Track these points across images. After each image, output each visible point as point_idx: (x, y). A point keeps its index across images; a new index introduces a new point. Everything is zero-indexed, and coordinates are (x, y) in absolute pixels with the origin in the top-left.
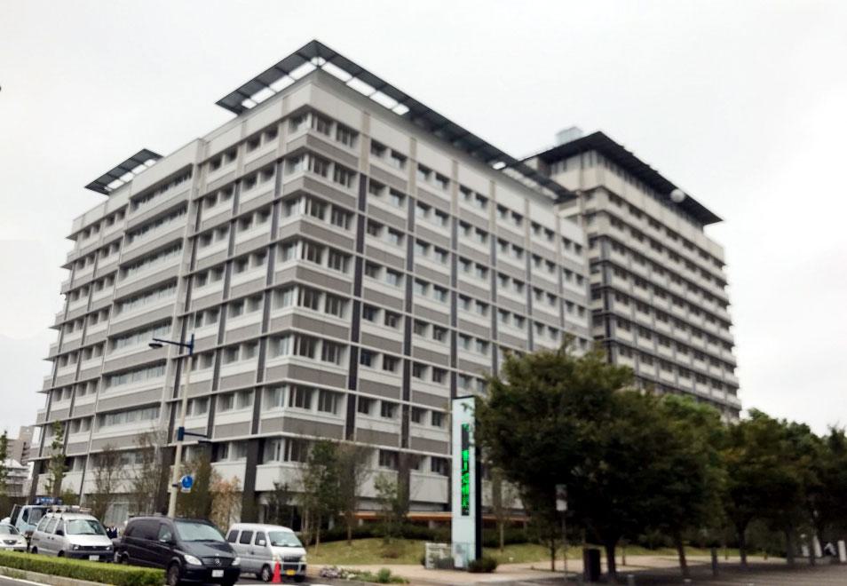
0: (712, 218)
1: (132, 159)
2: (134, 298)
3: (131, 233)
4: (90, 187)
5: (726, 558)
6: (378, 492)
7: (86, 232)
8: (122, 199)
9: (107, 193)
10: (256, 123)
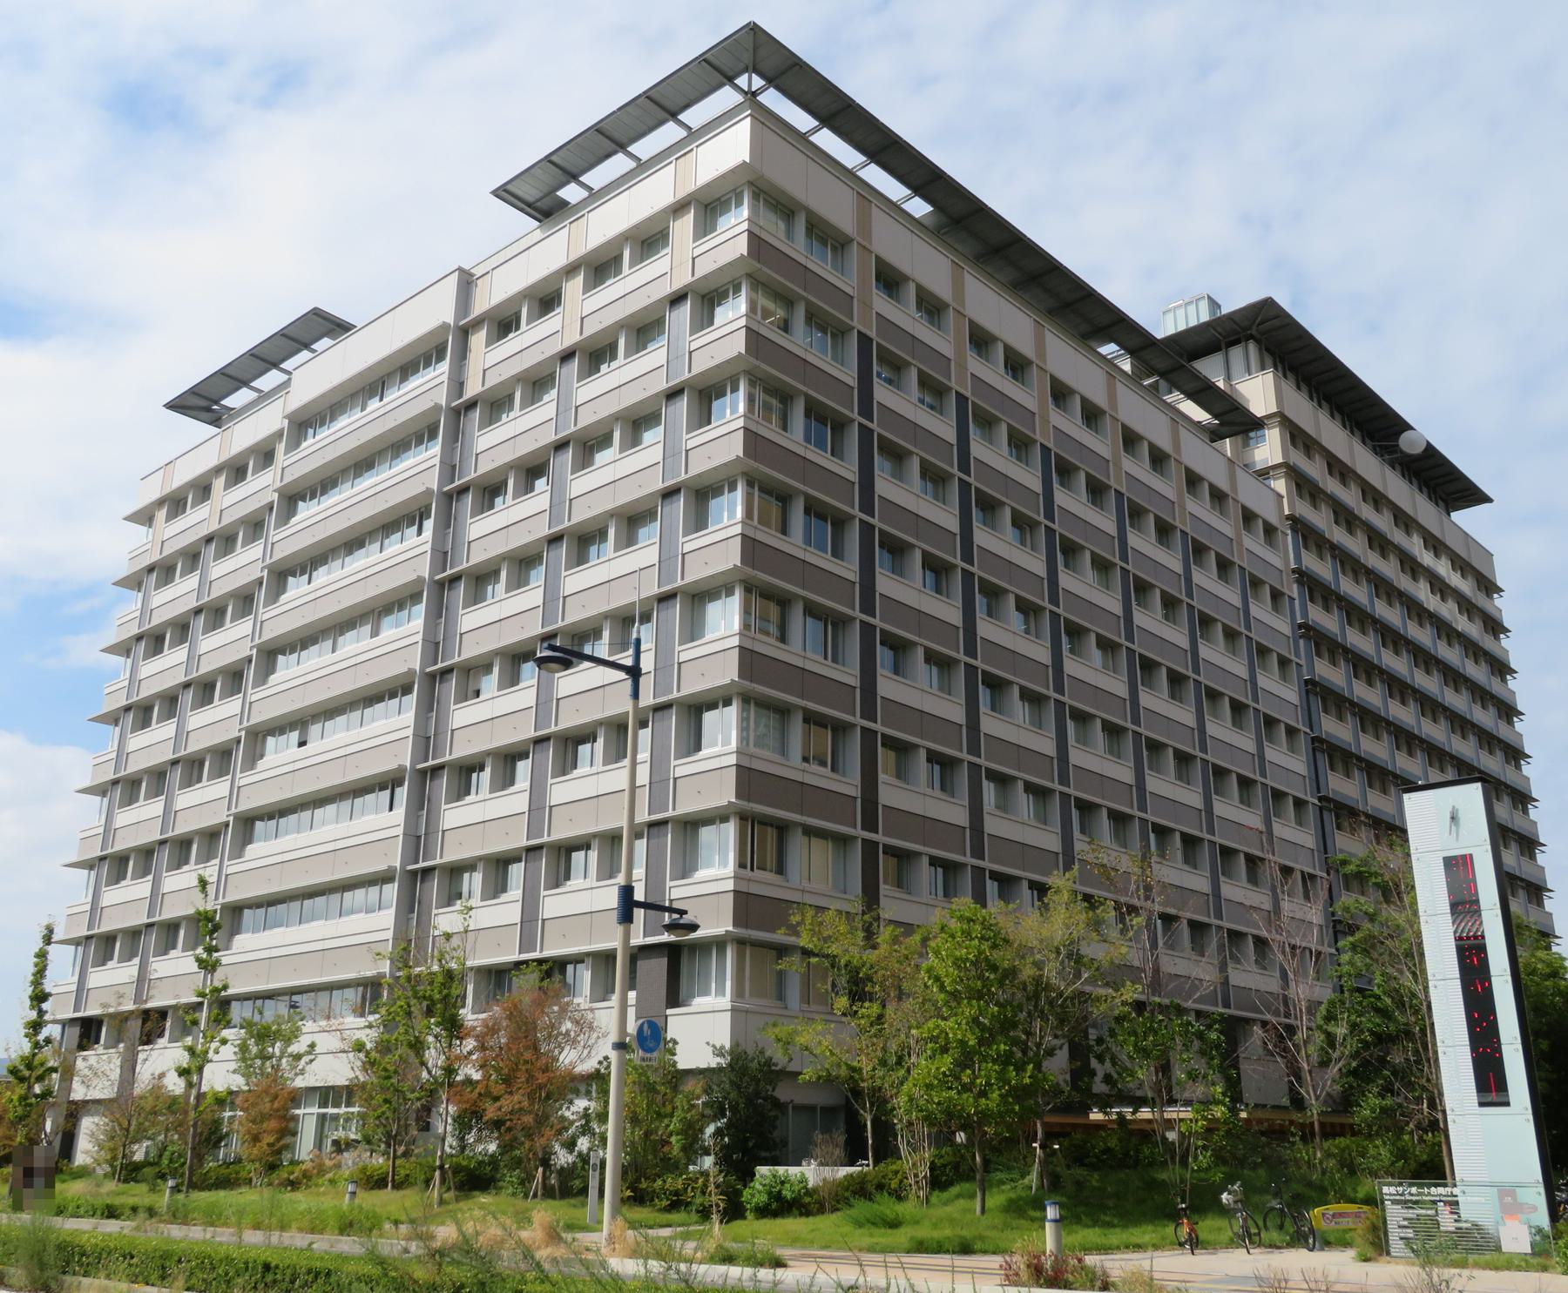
0: (1470, 495)
1: (283, 334)
2: (303, 640)
3: (291, 498)
4: (177, 406)
5: (787, 1170)
6: (719, 1060)
7: (175, 503)
8: (268, 421)
9: (216, 421)
10: (244, 435)
